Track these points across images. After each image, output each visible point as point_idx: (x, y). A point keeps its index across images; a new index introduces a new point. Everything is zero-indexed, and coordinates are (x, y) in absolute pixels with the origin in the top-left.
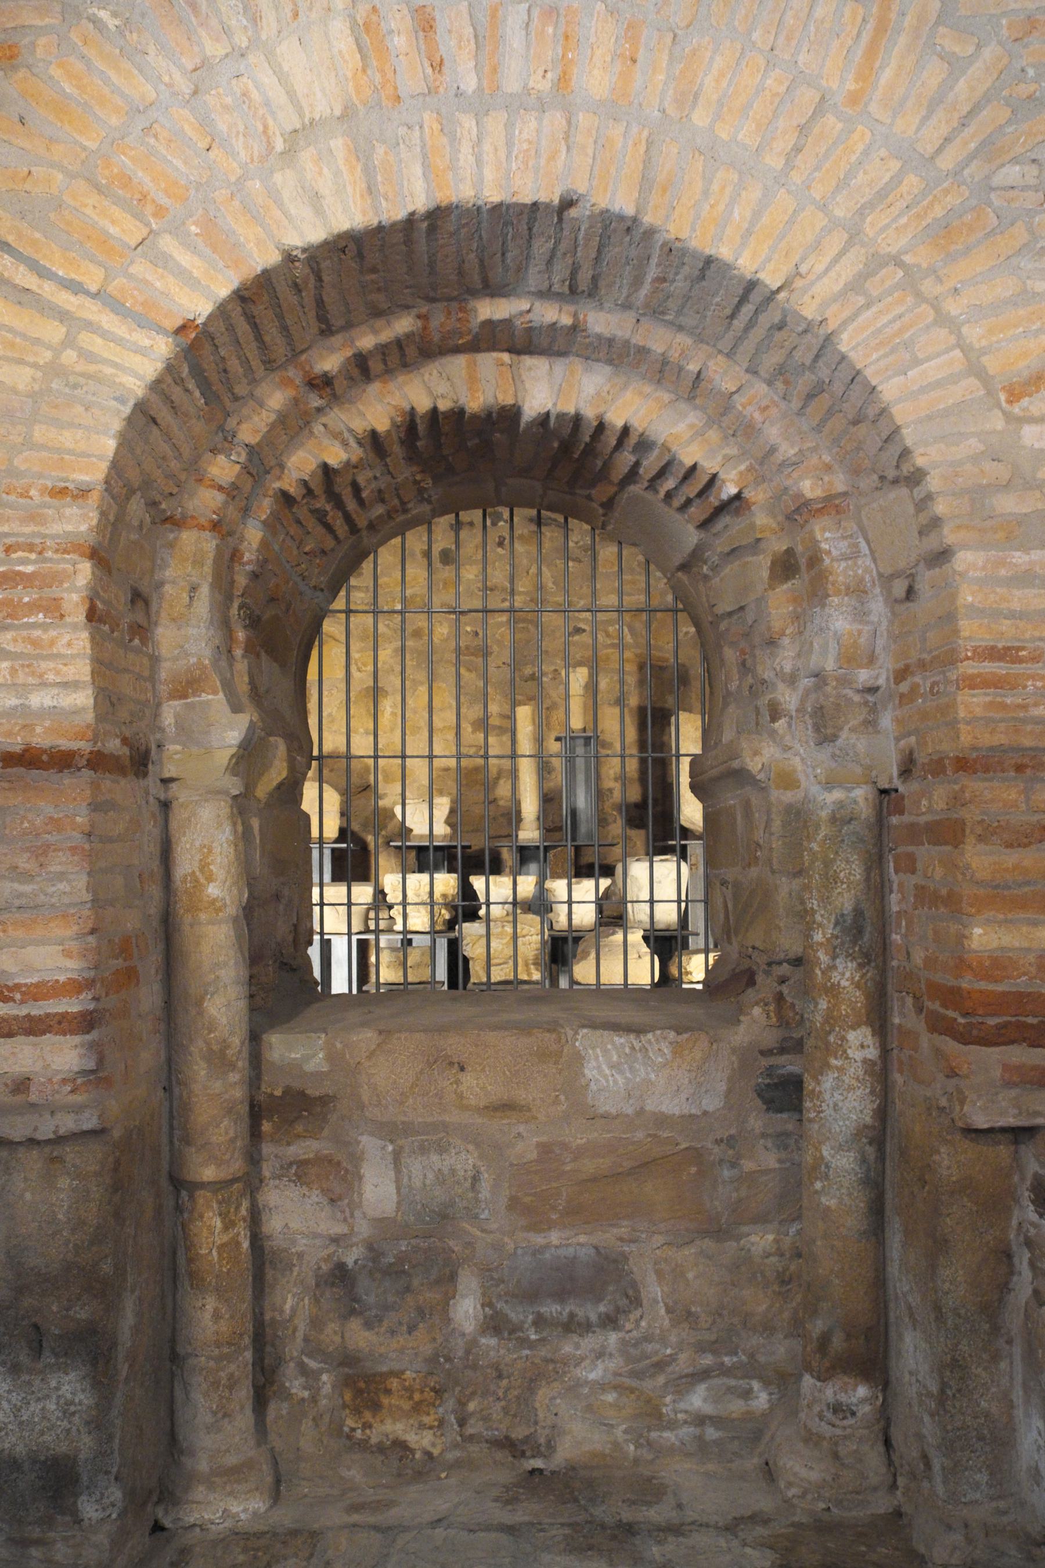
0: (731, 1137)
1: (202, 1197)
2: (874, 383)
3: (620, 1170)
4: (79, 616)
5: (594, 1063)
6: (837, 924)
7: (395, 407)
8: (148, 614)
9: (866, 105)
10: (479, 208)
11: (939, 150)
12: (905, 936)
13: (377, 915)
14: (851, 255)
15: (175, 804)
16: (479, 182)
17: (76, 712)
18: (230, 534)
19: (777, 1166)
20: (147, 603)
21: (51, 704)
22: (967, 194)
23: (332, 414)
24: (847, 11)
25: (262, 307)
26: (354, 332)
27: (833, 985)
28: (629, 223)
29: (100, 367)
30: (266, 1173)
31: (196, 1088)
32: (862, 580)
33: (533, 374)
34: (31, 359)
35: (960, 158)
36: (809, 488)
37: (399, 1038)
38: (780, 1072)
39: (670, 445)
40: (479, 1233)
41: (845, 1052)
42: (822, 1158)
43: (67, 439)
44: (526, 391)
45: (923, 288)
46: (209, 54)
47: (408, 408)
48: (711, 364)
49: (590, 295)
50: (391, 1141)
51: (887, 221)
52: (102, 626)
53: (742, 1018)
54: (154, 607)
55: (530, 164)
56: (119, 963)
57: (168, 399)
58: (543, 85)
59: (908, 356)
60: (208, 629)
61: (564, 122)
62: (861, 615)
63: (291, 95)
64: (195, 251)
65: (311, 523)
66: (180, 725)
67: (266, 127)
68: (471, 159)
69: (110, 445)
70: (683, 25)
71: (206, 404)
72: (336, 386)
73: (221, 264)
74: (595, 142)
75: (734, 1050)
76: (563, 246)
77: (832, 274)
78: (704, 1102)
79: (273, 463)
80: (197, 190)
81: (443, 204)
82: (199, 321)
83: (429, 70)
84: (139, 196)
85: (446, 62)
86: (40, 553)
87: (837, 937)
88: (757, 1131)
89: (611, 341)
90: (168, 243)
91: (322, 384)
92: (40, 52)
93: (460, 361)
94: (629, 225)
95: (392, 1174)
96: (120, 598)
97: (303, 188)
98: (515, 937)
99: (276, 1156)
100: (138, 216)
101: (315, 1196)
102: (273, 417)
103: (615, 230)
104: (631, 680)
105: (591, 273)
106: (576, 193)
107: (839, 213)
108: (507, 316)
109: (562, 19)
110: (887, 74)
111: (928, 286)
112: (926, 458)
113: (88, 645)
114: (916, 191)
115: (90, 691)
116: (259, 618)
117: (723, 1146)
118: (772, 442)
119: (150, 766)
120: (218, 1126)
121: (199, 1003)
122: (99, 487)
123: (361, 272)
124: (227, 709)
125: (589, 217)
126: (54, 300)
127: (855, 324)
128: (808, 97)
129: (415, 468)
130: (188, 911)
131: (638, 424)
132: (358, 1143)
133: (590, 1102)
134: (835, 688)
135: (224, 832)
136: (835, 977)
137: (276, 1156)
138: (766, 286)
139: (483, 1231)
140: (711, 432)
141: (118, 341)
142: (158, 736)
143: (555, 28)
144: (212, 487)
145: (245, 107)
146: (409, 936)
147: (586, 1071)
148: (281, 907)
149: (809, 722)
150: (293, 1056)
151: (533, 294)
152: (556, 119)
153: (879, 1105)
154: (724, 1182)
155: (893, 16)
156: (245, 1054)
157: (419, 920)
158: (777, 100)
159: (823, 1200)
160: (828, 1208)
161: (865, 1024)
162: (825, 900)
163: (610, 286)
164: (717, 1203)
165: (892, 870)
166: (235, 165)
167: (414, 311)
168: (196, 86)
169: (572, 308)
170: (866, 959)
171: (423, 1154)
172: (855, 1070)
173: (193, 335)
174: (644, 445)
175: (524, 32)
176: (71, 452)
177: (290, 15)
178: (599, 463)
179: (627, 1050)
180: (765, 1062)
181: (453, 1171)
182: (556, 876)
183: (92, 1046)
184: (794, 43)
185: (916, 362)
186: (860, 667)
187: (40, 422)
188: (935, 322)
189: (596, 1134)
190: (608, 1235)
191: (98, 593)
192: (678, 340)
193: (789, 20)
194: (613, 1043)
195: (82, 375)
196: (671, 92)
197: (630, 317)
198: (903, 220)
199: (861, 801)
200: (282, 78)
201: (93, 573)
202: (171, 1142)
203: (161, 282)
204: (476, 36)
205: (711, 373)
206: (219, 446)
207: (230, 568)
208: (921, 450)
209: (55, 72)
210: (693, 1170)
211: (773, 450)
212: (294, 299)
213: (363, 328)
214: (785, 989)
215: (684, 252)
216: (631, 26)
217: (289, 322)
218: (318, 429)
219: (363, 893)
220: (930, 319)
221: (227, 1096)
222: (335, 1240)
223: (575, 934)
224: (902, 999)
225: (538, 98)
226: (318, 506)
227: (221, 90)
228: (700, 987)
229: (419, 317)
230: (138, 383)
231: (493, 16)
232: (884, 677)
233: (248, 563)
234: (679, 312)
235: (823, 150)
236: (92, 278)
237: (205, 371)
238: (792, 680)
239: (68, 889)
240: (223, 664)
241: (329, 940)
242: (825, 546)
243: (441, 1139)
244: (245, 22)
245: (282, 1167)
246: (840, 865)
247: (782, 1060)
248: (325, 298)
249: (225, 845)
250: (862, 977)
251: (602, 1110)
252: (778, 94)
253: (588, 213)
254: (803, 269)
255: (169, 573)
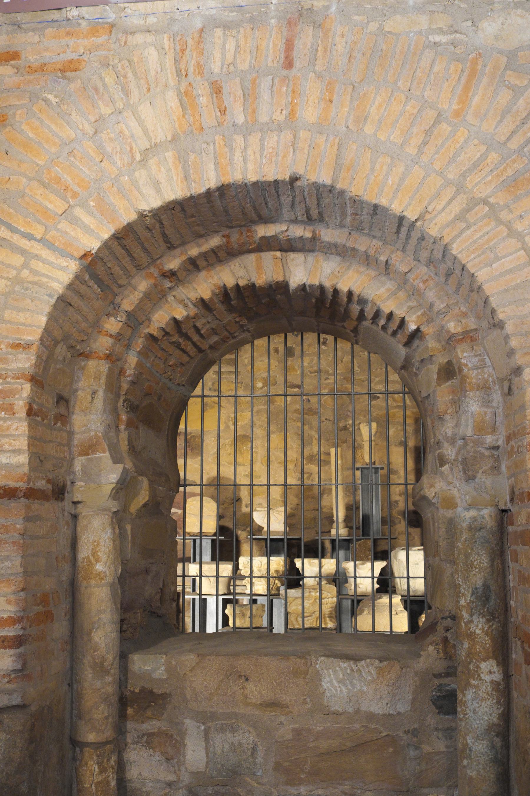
0: (415, 729)
1: (87, 751)
2: (472, 272)
3: (344, 748)
4: (22, 413)
5: (328, 679)
6: (473, 594)
7: (214, 284)
8: (68, 407)
9: (465, 116)
10: (246, 184)
11: (509, 139)
12: (515, 602)
13: (234, 583)
14: (459, 199)
15: (80, 517)
16: (245, 170)
17: (19, 466)
18: (118, 360)
19: (445, 750)
20: (67, 401)
21: (6, 462)
22: (527, 162)
23: (179, 290)
24: (452, 67)
25: (129, 241)
26: (187, 247)
27: (471, 632)
28: (330, 188)
29: (41, 278)
30: (129, 740)
31: (86, 684)
32: (487, 381)
33: (294, 262)
34: (5, 275)
35: (522, 142)
36: (453, 327)
37: (209, 660)
38: (447, 688)
39: (375, 301)
40: (256, 784)
41: (479, 675)
42: (467, 744)
43: (21, 317)
44: (291, 272)
45: (501, 217)
46: (103, 113)
47: (222, 284)
48: (393, 256)
49: (320, 221)
50: (204, 724)
51: (479, 179)
52: (37, 418)
53: (422, 653)
54: (72, 404)
55: (273, 160)
56: (40, 608)
57: (77, 292)
58: (281, 118)
59: (492, 255)
60: (102, 415)
61: (292, 137)
62: (487, 402)
63: (145, 132)
64: (92, 214)
65: (171, 349)
66: (85, 472)
67: (131, 148)
68: (241, 159)
69: (44, 320)
70: (358, 81)
71: (102, 291)
72: (179, 275)
73: (105, 221)
74: (309, 146)
75: (416, 674)
76: (298, 199)
77: (447, 210)
78: (398, 706)
79: (144, 318)
80: (94, 183)
81: (226, 183)
82: (93, 252)
83: (219, 114)
84: (64, 188)
85: (228, 109)
86: (5, 379)
87: (473, 602)
88: (432, 726)
89: (336, 245)
90: (78, 212)
91: (172, 275)
92: (17, 118)
93: (252, 257)
94: (331, 189)
95: (203, 744)
96: (49, 401)
97: (150, 179)
98: (321, 598)
99: (135, 730)
100: (64, 198)
101: (158, 756)
102: (141, 295)
103: (323, 191)
104: (410, 429)
105: (317, 211)
106: (298, 174)
107: (451, 176)
108: (274, 234)
109: (291, 83)
110: (477, 99)
111: (504, 215)
112: (504, 314)
113: (27, 430)
114: (496, 162)
115: (27, 455)
116: (138, 407)
117: (410, 735)
118: (430, 300)
119: (66, 495)
120: (97, 709)
121: (89, 634)
122: (37, 343)
123: (186, 218)
124: (110, 462)
125: (307, 185)
126: (18, 244)
127: (461, 238)
128: (430, 115)
129: (234, 315)
130: (84, 579)
131: (356, 291)
132: (184, 724)
133: (325, 702)
134: (473, 447)
135: (106, 533)
136: (473, 628)
137: (135, 730)
138: (409, 219)
139: (258, 783)
140: (400, 293)
141: (51, 264)
142: (72, 477)
143: (287, 88)
144: (106, 335)
145: (121, 139)
146: (254, 597)
147: (323, 684)
148: (149, 578)
149: (461, 467)
150: (146, 668)
151: (288, 221)
152: (287, 135)
153: (504, 711)
154: (410, 759)
155: (479, 67)
156: (116, 665)
157: (260, 587)
158: (412, 117)
159: (468, 772)
160: (471, 778)
161: (492, 658)
162: (466, 579)
163: (330, 216)
164: (406, 773)
165: (510, 561)
166: (115, 169)
167: (221, 234)
168: (96, 130)
169: (312, 228)
170: (492, 616)
171: (222, 733)
172: (486, 688)
173: (90, 259)
174: (362, 301)
175: (270, 91)
176: (23, 324)
177: (146, 90)
178: (342, 310)
179: (349, 671)
180: (436, 682)
181: (240, 744)
182: (347, 560)
183: (20, 656)
184: (422, 86)
185: (498, 259)
186: (487, 434)
187: (8, 309)
188: (509, 236)
189: (329, 724)
190: (336, 790)
191: (34, 400)
192: (373, 243)
193: (419, 73)
194: (340, 666)
195: (31, 282)
196: (351, 117)
197: (346, 231)
198: (490, 178)
199: (487, 518)
200: (140, 122)
201: (31, 390)
202: (72, 717)
203: (74, 232)
204: (244, 95)
205: (393, 262)
206: (111, 312)
207: (119, 379)
208: (502, 310)
209: (24, 127)
210: (391, 750)
211: (432, 306)
212: (149, 235)
213: (193, 244)
214: (449, 635)
215: (361, 202)
216: (329, 83)
217: (147, 246)
218: (171, 298)
219: (226, 569)
220: (505, 234)
221: (104, 691)
222: (169, 784)
223: (359, 598)
224: (516, 642)
225: (278, 124)
226: (174, 340)
227: (109, 131)
228: (389, 633)
229: (224, 236)
230: (60, 286)
231: (254, 83)
232: (502, 440)
233: (128, 376)
234: (371, 228)
235: (440, 142)
236: (38, 231)
237: (99, 275)
238: (452, 441)
239: (10, 565)
240: (112, 434)
241: (205, 599)
242: (463, 361)
243: (233, 724)
244: (122, 96)
245: (138, 737)
246: (474, 557)
247: (447, 680)
248: (166, 232)
249: (107, 541)
250: (489, 628)
251: (333, 709)
252: (413, 114)
253: (306, 184)
254: (430, 208)
255: (81, 384)
